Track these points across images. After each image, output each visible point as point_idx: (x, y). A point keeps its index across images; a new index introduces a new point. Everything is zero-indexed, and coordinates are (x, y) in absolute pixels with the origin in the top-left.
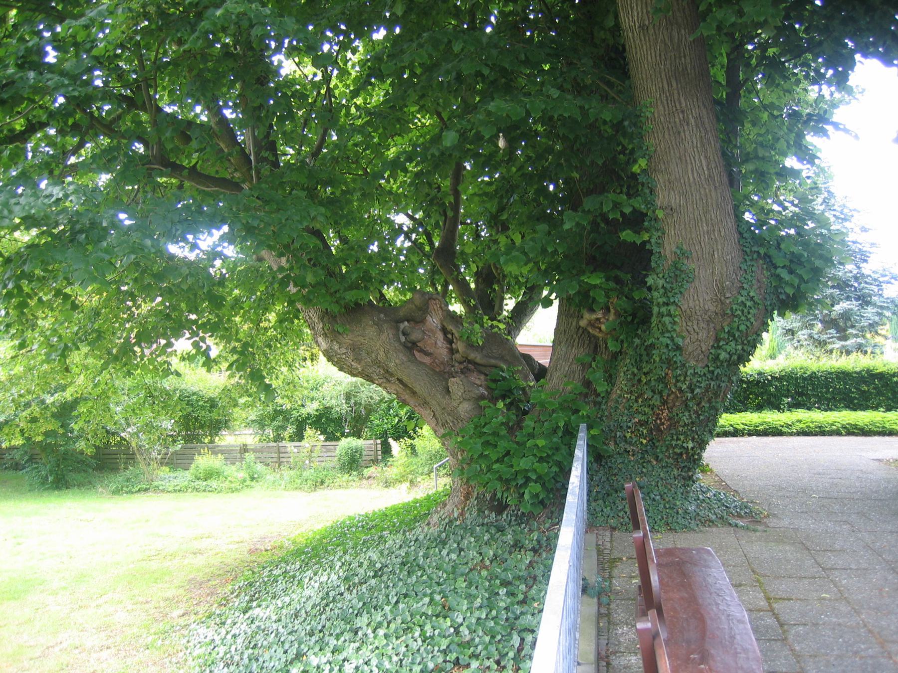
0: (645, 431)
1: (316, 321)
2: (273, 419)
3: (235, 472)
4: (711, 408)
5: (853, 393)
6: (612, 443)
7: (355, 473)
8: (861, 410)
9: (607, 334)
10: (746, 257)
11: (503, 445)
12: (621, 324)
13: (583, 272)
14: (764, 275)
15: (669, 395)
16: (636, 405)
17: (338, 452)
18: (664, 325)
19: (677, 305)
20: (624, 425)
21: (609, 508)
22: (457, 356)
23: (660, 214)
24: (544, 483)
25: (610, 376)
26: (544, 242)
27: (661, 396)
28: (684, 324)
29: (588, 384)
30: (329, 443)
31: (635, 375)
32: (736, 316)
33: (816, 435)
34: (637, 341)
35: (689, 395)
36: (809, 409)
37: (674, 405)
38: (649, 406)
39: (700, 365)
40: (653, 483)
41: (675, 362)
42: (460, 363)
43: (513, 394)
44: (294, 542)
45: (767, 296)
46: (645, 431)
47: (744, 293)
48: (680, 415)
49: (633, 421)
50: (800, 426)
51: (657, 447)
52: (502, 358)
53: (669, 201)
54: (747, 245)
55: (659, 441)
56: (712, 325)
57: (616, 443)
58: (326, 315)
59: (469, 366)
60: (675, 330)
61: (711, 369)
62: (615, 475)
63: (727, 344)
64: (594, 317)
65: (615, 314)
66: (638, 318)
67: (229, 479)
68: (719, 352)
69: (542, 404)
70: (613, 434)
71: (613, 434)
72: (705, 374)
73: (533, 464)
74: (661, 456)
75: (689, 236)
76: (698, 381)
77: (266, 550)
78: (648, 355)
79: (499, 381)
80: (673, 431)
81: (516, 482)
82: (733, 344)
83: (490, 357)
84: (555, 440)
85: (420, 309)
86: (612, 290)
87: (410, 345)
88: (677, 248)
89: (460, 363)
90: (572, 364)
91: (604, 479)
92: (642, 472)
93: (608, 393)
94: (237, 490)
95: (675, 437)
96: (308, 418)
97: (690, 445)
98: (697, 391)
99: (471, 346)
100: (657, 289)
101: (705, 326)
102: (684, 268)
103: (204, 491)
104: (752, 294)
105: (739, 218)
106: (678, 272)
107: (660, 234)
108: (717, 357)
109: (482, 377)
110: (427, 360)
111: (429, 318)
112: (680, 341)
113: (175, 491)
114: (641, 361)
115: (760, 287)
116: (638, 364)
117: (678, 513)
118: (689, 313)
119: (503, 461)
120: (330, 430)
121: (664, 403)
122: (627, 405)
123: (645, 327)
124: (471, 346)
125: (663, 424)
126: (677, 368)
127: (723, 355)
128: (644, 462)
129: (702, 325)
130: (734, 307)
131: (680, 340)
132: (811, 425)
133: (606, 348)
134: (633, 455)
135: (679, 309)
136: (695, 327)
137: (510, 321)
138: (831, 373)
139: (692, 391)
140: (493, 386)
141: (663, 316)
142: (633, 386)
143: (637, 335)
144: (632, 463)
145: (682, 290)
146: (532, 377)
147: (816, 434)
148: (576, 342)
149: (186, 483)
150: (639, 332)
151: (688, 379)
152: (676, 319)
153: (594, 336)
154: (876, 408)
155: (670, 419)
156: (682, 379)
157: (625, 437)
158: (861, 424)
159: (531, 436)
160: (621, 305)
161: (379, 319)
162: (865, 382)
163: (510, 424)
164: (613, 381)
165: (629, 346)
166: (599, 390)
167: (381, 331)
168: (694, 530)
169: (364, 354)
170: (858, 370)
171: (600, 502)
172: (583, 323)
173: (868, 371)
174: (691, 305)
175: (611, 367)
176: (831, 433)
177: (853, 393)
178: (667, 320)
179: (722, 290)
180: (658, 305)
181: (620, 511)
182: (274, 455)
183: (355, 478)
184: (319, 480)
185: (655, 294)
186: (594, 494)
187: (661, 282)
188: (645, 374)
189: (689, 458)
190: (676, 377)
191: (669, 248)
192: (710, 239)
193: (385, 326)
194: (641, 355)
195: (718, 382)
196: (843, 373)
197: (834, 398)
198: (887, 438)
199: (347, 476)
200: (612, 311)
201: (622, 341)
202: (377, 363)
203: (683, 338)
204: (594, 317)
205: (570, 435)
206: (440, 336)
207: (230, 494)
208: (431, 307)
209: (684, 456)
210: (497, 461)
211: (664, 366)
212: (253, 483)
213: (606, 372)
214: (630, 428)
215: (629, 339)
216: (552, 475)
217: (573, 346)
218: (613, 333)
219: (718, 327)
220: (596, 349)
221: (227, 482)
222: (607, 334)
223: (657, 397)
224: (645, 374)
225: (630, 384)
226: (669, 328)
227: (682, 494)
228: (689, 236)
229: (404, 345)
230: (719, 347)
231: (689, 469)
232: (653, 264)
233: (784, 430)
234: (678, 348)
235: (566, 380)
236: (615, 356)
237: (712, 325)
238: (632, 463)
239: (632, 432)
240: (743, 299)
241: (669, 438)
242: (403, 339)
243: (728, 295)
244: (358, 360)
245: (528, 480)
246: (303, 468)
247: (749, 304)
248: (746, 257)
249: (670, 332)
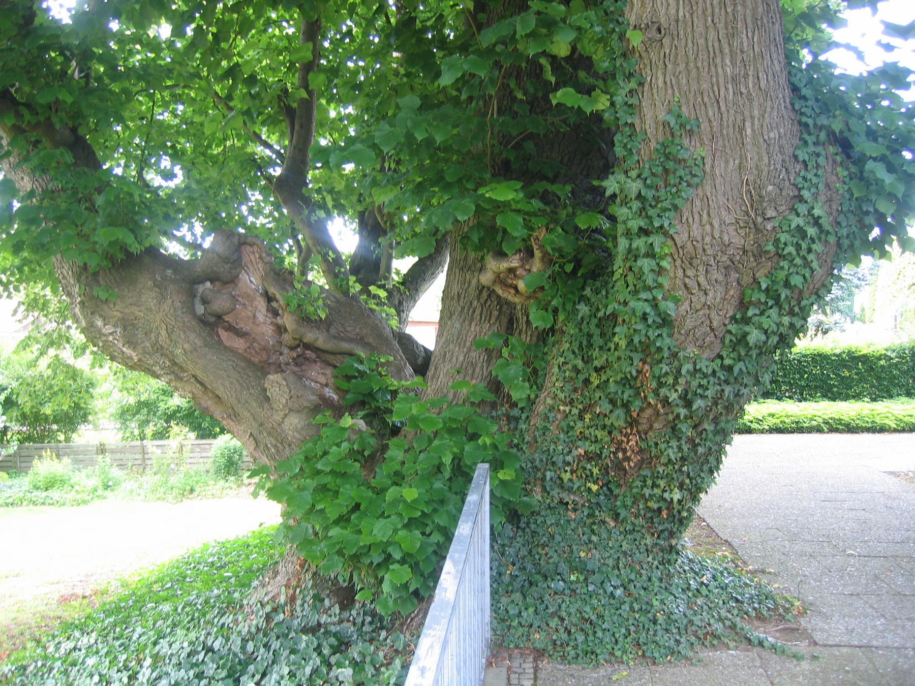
0: (596, 471)
1: (72, 282)
2: (138, 412)
3: (86, 479)
4: (716, 433)
5: (832, 379)
6: (538, 489)
7: (233, 478)
8: (842, 400)
9: (529, 298)
10: (805, 136)
11: (350, 492)
12: (553, 278)
13: (481, 183)
14: (838, 175)
15: (642, 410)
16: (580, 424)
17: (211, 453)
18: (640, 276)
19: (666, 234)
20: (559, 460)
21: (531, 610)
22: (286, 337)
23: (636, 39)
24: (417, 564)
25: (535, 372)
26: (409, 123)
27: (628, 411)
28: (680, 273)
29: (496, 386)
30: (204, 441)
31: (578, 371)
32: (784, 257)
33: (792, 432)
34: (584, 309)
35: (683, 412)
36: (779, 399)
37: (651, 427)
38: (604, 427)
39: (705, 355)
40: (610, 562)
41: (659, 349)
42: (292, 348)
43: (375, 399)
44: (125, 585)
45: (841, 218)
46: (596, 471)
47: (802, 209)
48: (663, 446)
49: (575, 453)
50: (771, 422)
51: (616, 497)
52: (361, 341)
53: (654, 11)
54: (808, 112)
55: (619, 486)
56: (734, 275)
57: (544, 488)
58: (85, 274)
59: (305, 354)
60: (660, 286)
61: (727, 362)
62: (544, 546)
63: (762, 313)
64: (504, 265)
65: (542, 259)
66: (585, 268)
67: (76, 487)
68: (747, 329)
69: (414, 420)
70: (539, 475)
71: (539, 475)
72: (714, 372)
73: (396, 531)
74: (623, 513)
75: (694, 87)
76: (700, 386)
77: (84, 597)
78: (602, 335)
79: (356, 377)
80: (646, 472)
81: (373, 560)
82: (774, 312)
83: (342, 339)
84: (438, 485)
85: (226, 260)
86: (534, 214)
87: (213, 319)
88: (669, 112)
89: (292, 348)
90: (469, 350)
91: (524, 552)
92: (590, 541)
93: (531, 402)
94: (85, 502)
95: (649, 482)
96: (175, 412)
97: (677, 496)
98: (698, 403)
99: (306, 320)
100: (625, 203)
101: (721, 278)
102: (682, 155)
103: (43, 503)
104: (817, 212)
105: (791, 56)
106: (671, 165)
107: (633, 85)
108: (742, 339)
109: (329, 371)
110: (239, 344)
111: (244, 276)
112: (669, 307)
113: (7, 505)
114: (590, 345)
115: (830, 200)
116: (584, 350)
117: (655, 622)
118: (685, 255)
119: (348, 520)
120: (205, 425)
121: (633, 423)
122: (563, 424)
123: (598, 284)
124: (306, 320)
125: (628, 459)
126: (660, 361)
127: (755, 336)
128: (592, 524)
129: (716, 275)
130: (783, 237)
131: (671, 305)
132: (787, 421)
133: (528, 322)
134: (575, 510)
135: (670, 242)
136: (702, 279)
137: (402, 288)
138: (805, 356)
139: (688, 404)
140: (345, 385)
141: (636, 258)
142: (575, 390)
143: (582, 298)
144: (573, 525)
145: (677, 201)
146: (409, 370)
147: (792, 431)
148: (478, 312)
149: (21, 494)
150: (587, 292)
151: (682, 381)
152: (664, 264)
153: (508, 303)
154: (857, 397)
155: (641, 450)
156: (671, 380)
157: (561, 479)
158: (846, 419)
159: (398, 479)
160: (552, 242)
161: (165, 278)
162: (845, 366)
163: (366, 453)
164: (540, 381)
165: (567, 318)
166: (515, 395)
167: (162, 298)
168: (686, 658)
169: (140, 334)
170: (837, 351)
171: (517, 596)
172: (486, 278)
173: (849, 353)
174: (696, 232)
175: (536, 357)
176: (810, 430)
177: (832, 379)
178: (646, 264)
179: (757, 202)
180: (628, 234)
181: (553, 615)
182: (137, 456)
183: (232, 485)
184: (188, 488)
185: (622, 212)
186: (506, 579)
187: (634, 187)
188: (597, 370)
189: (671, 516)
190: (659, 378)
191: (652, 115)
192: (738, 93)
193: (171, 288)
194: (590, 336)
195: (737, 387)
196: (820, 355)
197: (807, 385)
198: (878, 436)
199: (222, 482)
200: (538, 254)
201: (555, 311)
202: (158, 349)
203: (677, 301)
204: (504, 265)
205: (462, 475)
206: (261, 304)
207: (75, 507)
208: (245, 259)
209: (664, 514)
210: (336, 522)
211: (637, 357)
212: (108, 493)
213: (527, 364)
214: (568, 464)
215: (569, 307)
216: (431, 550)
217: (472, 320)
218: (540, 295)
219: (747, 280)
220: (511, 326)
221: (73, 492)
222: (529, 298)
223: (620, 412)
224: (597, 370)
225: (568, 387)
226: (650, 282)
227: (661, 580)
228: (694, 87)
229: (202, 321)
230: (746, 321)
231: (672, 534)
232: (619, 151)
233: (754, 426)
234: (666, 321)
235: (459, 378)
236: (543, 336)
237: (734, 275)
238: (573, 525)
239: (572, 472)
240: (800, 221)
241: (638, 483)
242: (200, 309)
243: (770, 213)
244: (131, 342)
245: (388, 558)
246: (170, 472)
247: (811, 231)
248: (805, 136)
249: (650, 289)
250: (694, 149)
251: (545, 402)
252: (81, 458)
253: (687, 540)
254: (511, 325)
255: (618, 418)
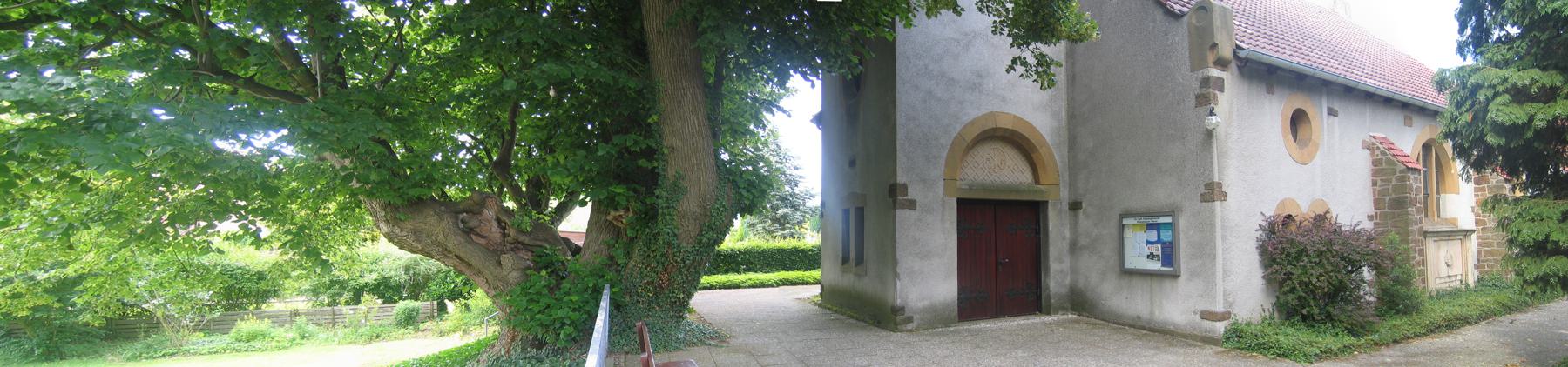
3: (281, 333)
11: (544, 301)
29: (611, 258)
52: (546, 241)
59: (518, 246)
66: (649, 216)
69: (576, 272)
81: (555, 327)
99: (521, 231)
105: (717, 156)
110: (483, 241)
116: (648, 245)
128: (650, 308)
167: (441, 219)
191: (671, 172)
205: (597, 292)
246: (359, 325)
250: (685, 184)
251: (632, 263)
252: (278, 320)
253: (689, 318)
254: (618, 234)
255: (660, 268)
